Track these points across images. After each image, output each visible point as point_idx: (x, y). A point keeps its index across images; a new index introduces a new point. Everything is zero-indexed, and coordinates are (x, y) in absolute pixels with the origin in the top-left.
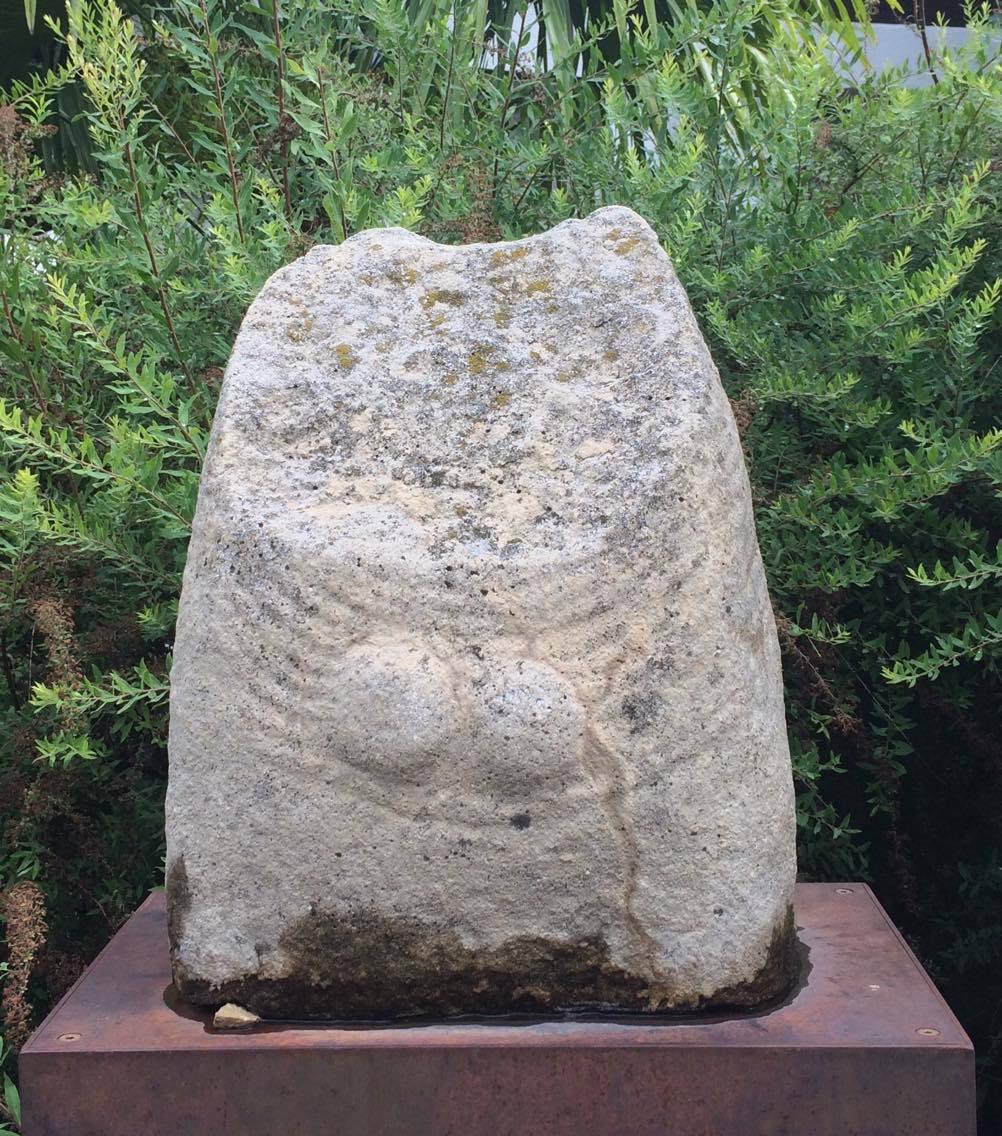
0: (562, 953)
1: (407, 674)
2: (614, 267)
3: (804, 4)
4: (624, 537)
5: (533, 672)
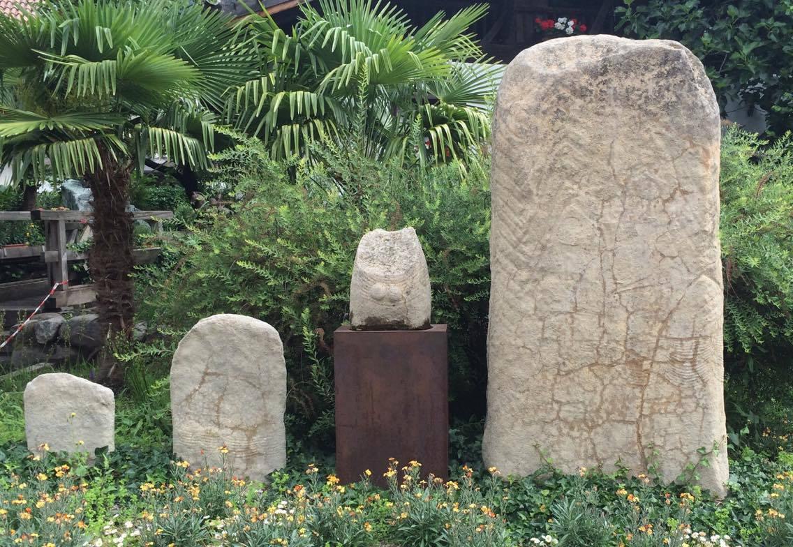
0: (399, 322)
1: (381, 288)
2: (409, 236)
3: (315, 4)
4: (407, 272)
5: (396, 288)
